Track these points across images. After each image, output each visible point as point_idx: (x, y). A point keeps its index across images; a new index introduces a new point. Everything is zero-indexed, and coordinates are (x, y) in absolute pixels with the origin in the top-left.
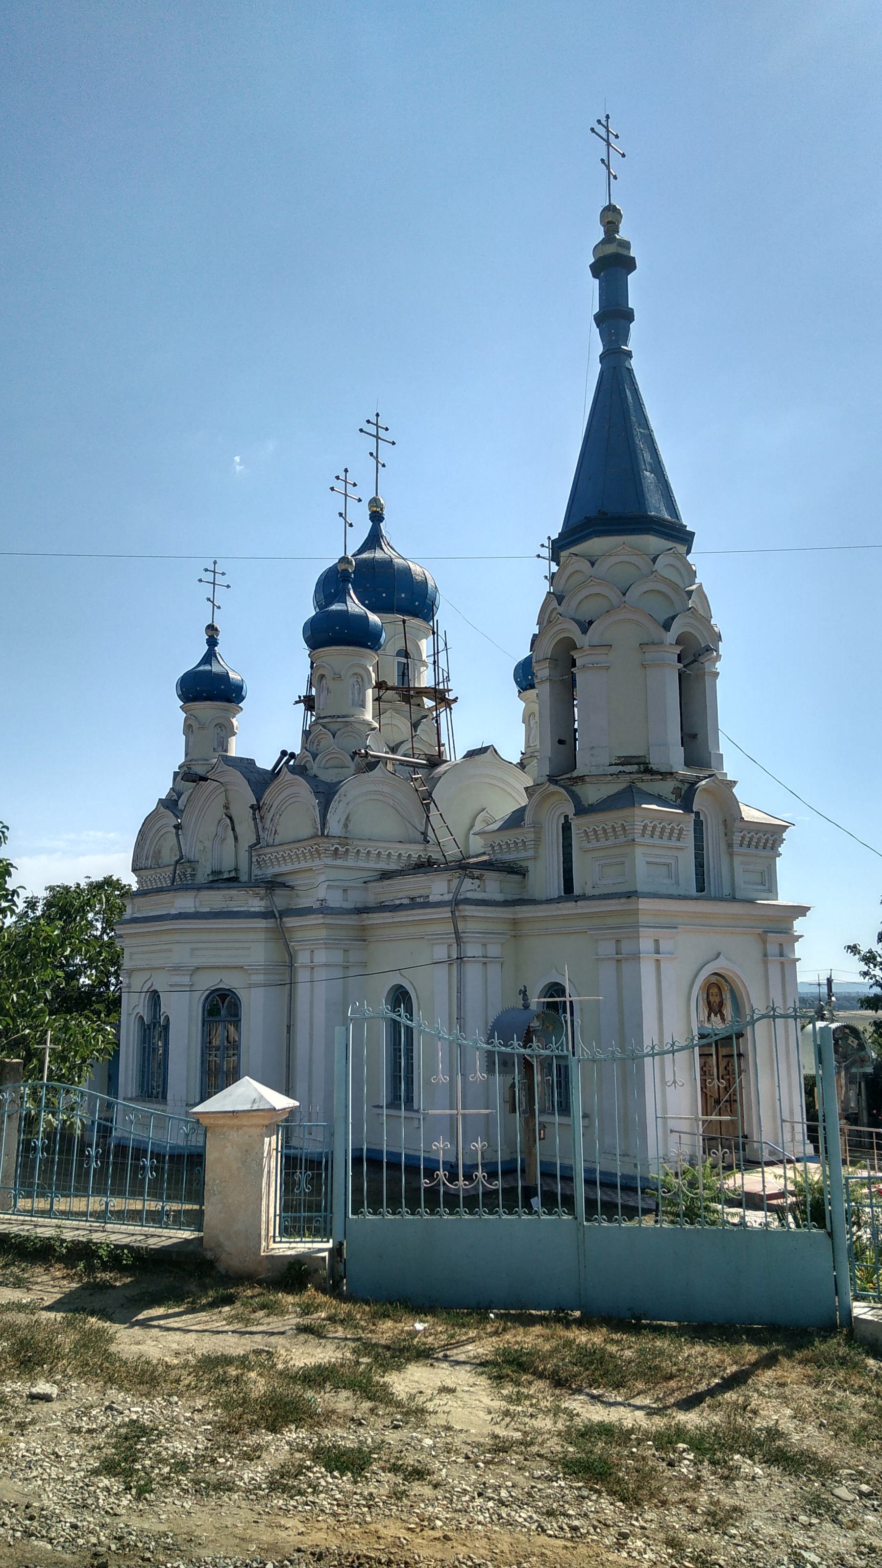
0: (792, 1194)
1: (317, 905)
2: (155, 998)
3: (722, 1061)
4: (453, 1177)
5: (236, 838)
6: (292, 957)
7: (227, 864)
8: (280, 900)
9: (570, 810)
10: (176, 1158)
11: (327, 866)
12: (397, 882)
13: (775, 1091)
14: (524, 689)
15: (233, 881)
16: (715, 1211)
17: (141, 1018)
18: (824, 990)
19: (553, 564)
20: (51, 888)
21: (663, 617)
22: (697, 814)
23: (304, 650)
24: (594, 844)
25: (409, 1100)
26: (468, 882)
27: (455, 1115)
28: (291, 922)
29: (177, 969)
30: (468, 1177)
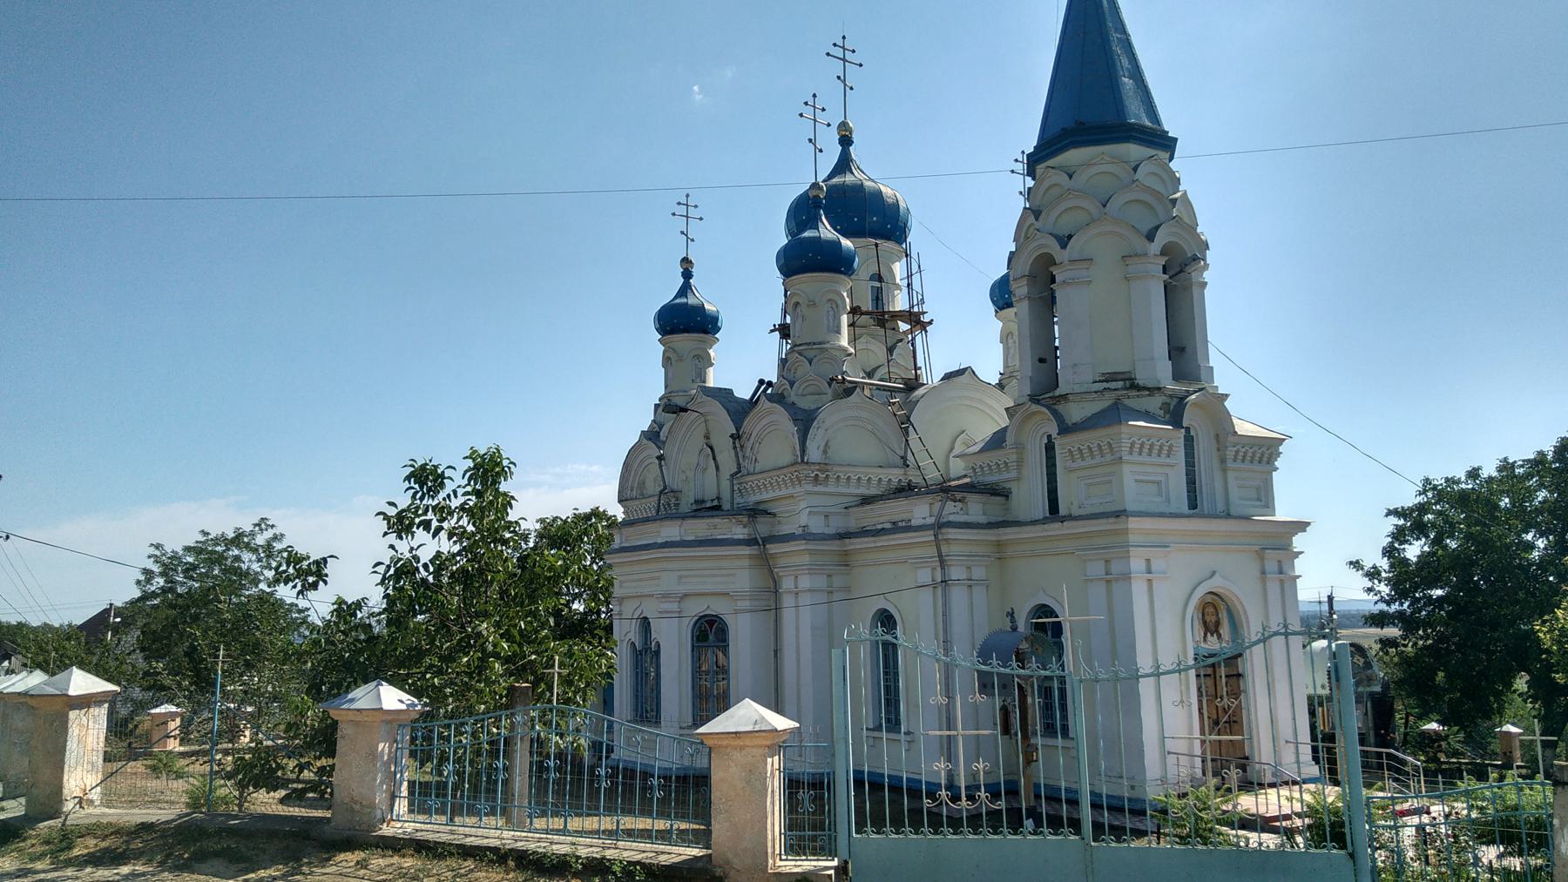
0: (1299, 815)
1: (800, 532)
2: (645, 624)
3: (1221, 683)
4: (955, 798)
5: (717, 468)
6: (776, 583)
7: (710, 493)
8: (763, 527)
9: (1053, 429)
10: (683, 779)
11: (809, 493)
12: (878, 507)
13: (1278, 715)
14: (1001, 308)
15: (716, 509)
16: (1220, 834)
17: (633, 644)
18: (1325, 607)
19: (1028, 179)
20: (542, 521)
21: (1146, 227)
22: (1188, 429)
23: (777, 278)
24: (1080, 463)
25: (1065, 729)
26: (950, 504)
27: (946, 738)
28: (773, 548)
29: (665, 596)
30: (970, 798)
